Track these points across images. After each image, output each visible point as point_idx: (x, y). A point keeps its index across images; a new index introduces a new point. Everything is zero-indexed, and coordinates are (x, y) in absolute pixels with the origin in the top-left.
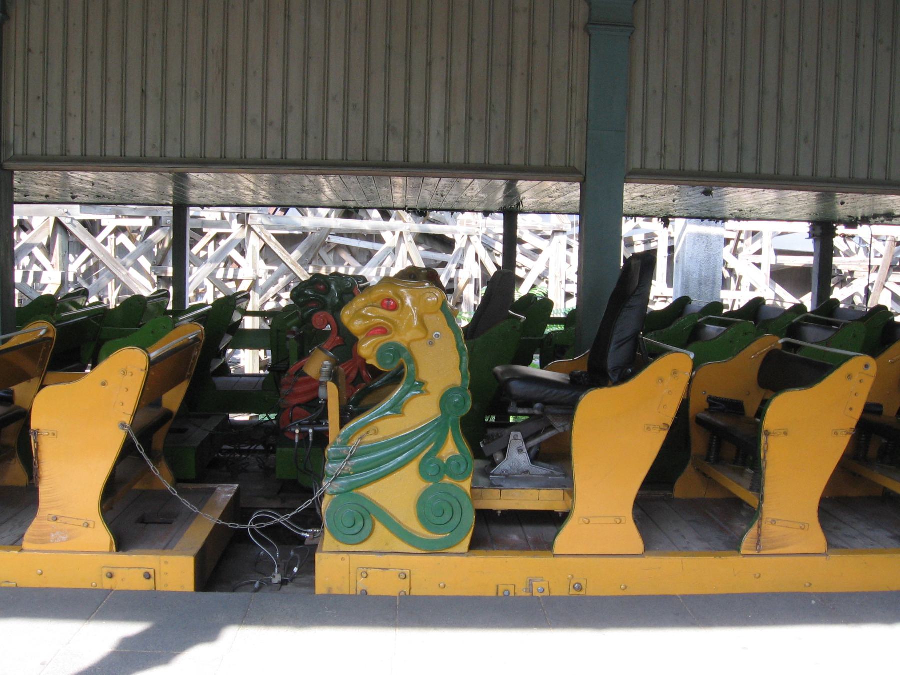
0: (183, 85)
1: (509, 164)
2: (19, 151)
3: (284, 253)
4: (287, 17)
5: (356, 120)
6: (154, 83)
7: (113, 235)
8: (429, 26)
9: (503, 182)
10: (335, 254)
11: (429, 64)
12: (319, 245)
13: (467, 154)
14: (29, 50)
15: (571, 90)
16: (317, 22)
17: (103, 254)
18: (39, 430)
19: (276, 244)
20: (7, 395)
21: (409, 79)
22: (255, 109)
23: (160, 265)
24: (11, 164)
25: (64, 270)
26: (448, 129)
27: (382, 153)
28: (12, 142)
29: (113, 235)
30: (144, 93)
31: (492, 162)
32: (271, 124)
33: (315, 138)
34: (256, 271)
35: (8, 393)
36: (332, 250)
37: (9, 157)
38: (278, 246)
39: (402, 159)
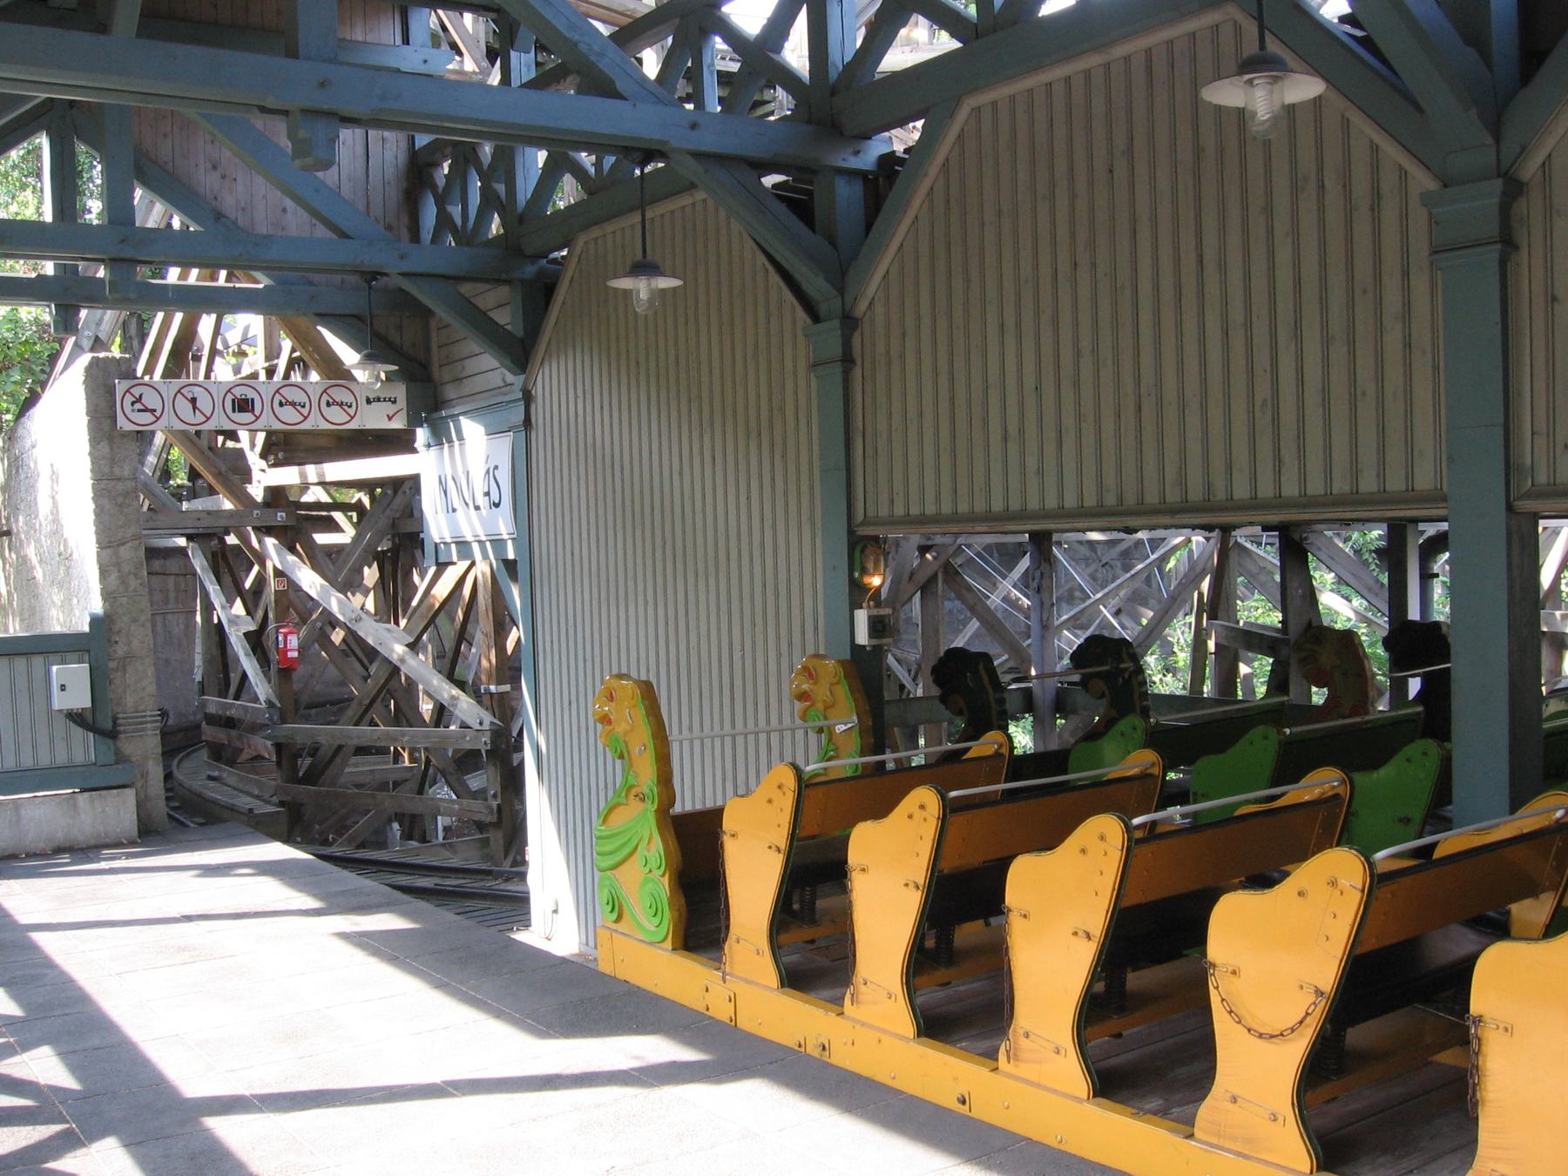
2: (1542, 478)
14: (1554, 299)
18: (1481, 1016)
20: (1498, 916)
24: (1526, 502)
28: (1528, 461)
35: (1501, 914)
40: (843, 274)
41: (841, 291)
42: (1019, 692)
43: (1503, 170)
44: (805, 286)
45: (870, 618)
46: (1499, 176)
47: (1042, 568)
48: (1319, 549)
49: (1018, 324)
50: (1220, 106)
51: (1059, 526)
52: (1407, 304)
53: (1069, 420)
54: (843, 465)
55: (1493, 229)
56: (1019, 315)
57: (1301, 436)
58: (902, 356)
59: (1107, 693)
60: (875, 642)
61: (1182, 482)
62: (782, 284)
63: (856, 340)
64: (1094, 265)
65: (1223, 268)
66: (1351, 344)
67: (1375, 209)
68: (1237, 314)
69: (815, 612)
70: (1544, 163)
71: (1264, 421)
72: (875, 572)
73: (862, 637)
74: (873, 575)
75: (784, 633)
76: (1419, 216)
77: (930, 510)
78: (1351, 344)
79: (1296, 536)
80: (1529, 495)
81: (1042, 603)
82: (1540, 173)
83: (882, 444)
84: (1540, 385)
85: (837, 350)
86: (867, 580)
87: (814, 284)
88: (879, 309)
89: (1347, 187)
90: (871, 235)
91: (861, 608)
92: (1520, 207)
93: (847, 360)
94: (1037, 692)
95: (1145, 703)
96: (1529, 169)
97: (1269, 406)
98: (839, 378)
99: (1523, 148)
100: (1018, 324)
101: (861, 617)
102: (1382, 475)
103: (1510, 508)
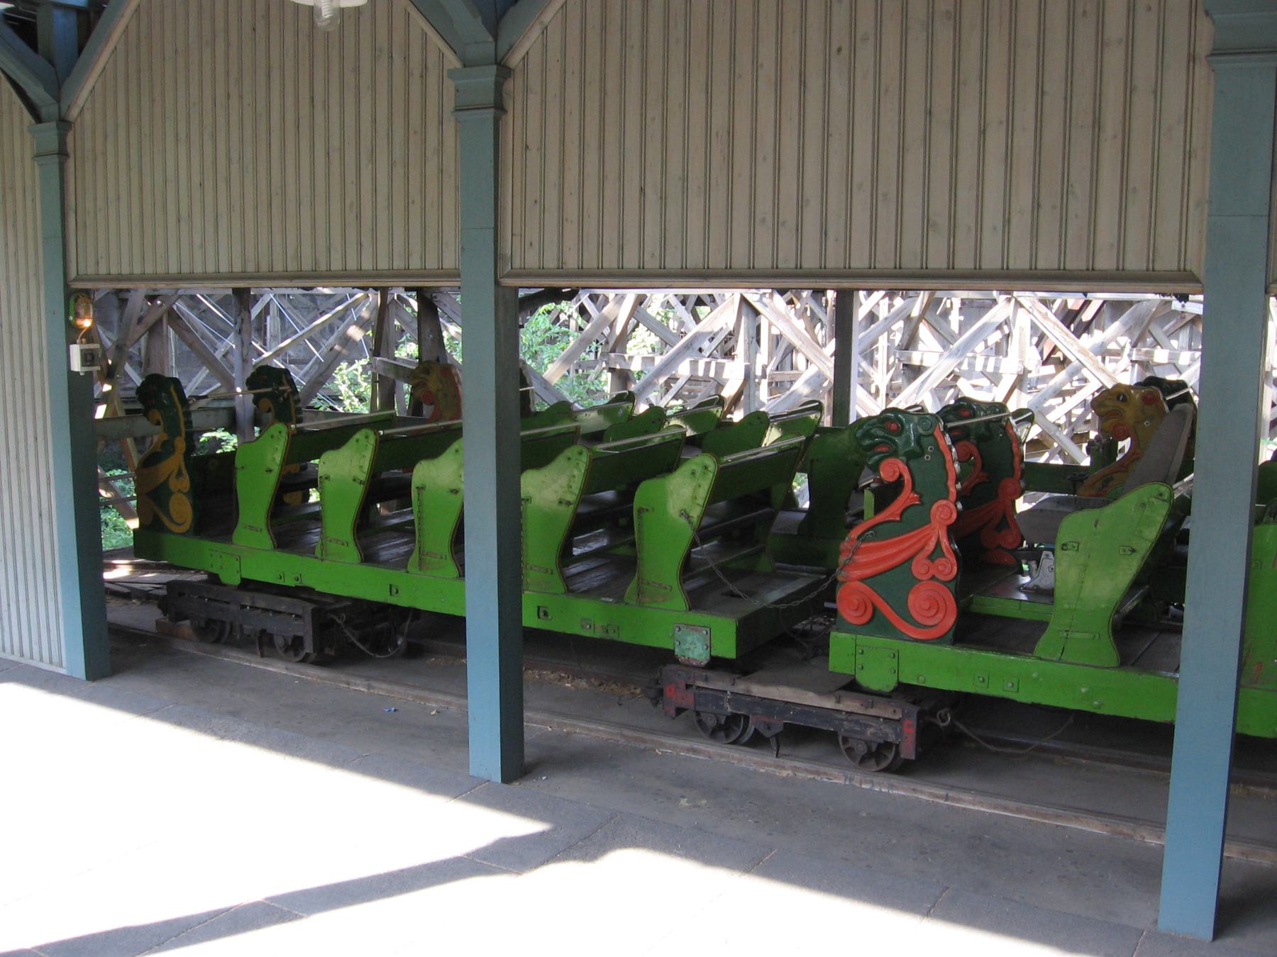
0: (685, 179)
1: (1093, 269)
2: (517, 264)
3: (1067, 335)
4: (803, 83)
5: (887, 214)
6: (653, 178)
7: (887, 298)
8: (983, 77)
9: (538, 409)
10: (1192, 328)
11: (983, 132)
12: (1148, 319)
13: (1034, 256)
14: (527, 147)
15: (1188, 156)
16: (839, 89)
17: (801, 340)
19: (1055, 324)
21: (955, 154)
22: (764, 207)
23: (907, 349)
25: (749, 361)
26: (1007, 222)
27: (919, 258)
29: (887, 298)
30: (642, 190)
31: (1068, 266)
32: (784, 223)
33: (837, 240)
34: (1022, 362)
36: (1186, 324)
37: (506, 272)
38: (1058, 326)
39: (945, 266)
40: (60, 87)
41: (58, 100)
42: (225, 411)
43: (499, 59)
44: (30, 94)
45: (82, 351)
46: (496, 64)
47: (242, 315)
48: (445, 305)
49: (188, 136)
50: (298, 4)
51: (395, 284)
52: (441, 142)
53: (223, 208)
54: (59, 234)
55: (490, 98)
56: (188, 128)
57: (374, 230)
58: (104, 154)
59: (272, 409)
60: (86, 369)
61: (299, 257)
62: (12, 90)
63: (70, 139)
64: (241, 97)
65: (326, 106)
66: (407, 166)
67: (423, 76)
68: (335, 142)
69: (40, 343)
70: (524, 57)
71: (351, 218)
72: (86, 316)
73: (76, 365)
74: (84, 318)
75: (17, 365)
76: (450, 85)
77: (125, 271)
78: (407, 166)
79: (428, 296)
80: (508, 276)
81: (243, 343)
82: (521, 64)
83: (89, 220)
84: (517, 201)
85: (54, 146)
86: (79, 322)
87: (37, 92)
88: (88, 116)
89: (406, 59)
90: (81, 57)
91: (75, 343)
92: (509, 85)
93: (63, 153)
94: (239, 410)
95: (300, 416)
96: (515, 60)
97: (355, 206)
98: (56, 168)
99: (511, 47)
100: (188, 136)
101: (75, 350)
102: (423, 258)
103: (497, 283)
